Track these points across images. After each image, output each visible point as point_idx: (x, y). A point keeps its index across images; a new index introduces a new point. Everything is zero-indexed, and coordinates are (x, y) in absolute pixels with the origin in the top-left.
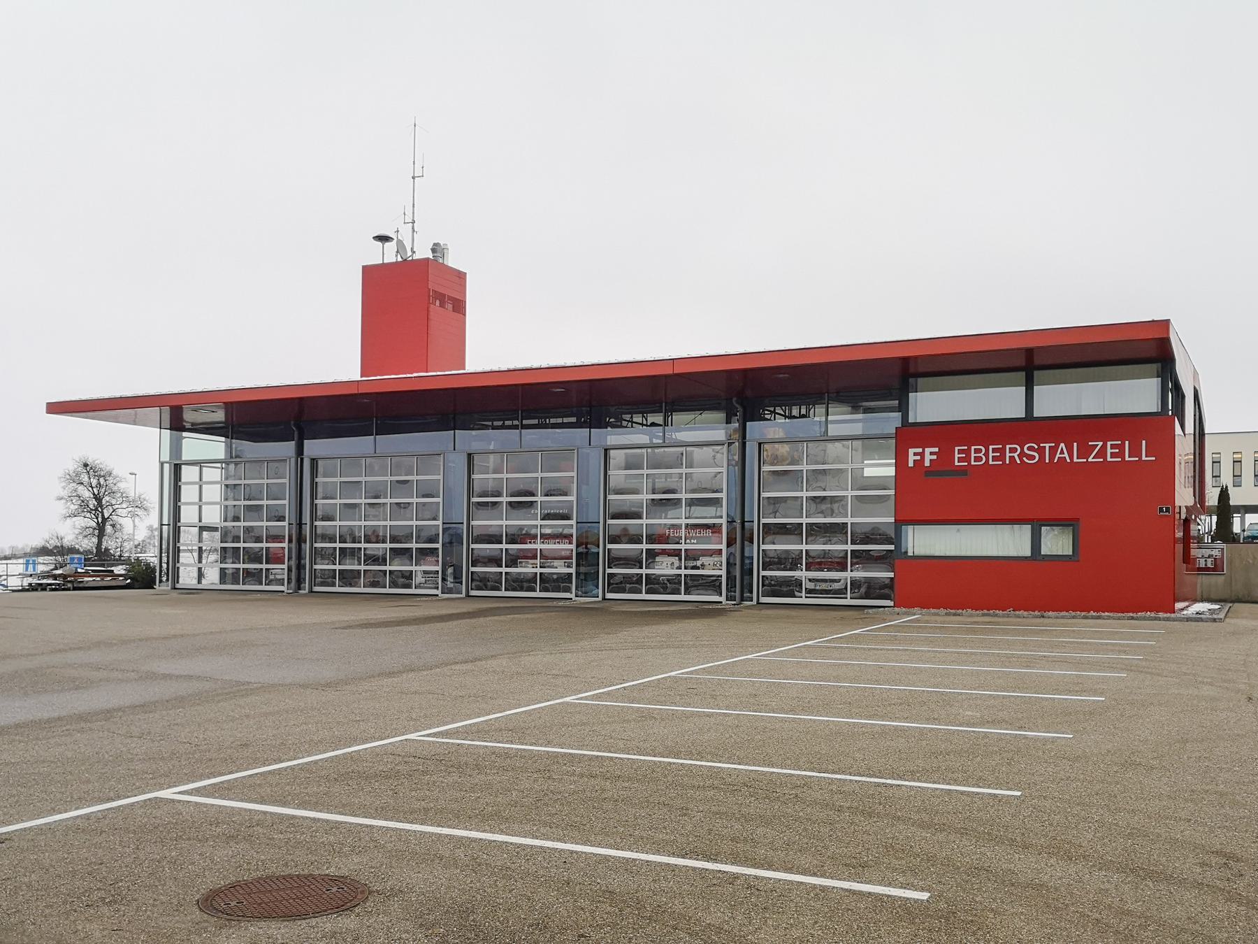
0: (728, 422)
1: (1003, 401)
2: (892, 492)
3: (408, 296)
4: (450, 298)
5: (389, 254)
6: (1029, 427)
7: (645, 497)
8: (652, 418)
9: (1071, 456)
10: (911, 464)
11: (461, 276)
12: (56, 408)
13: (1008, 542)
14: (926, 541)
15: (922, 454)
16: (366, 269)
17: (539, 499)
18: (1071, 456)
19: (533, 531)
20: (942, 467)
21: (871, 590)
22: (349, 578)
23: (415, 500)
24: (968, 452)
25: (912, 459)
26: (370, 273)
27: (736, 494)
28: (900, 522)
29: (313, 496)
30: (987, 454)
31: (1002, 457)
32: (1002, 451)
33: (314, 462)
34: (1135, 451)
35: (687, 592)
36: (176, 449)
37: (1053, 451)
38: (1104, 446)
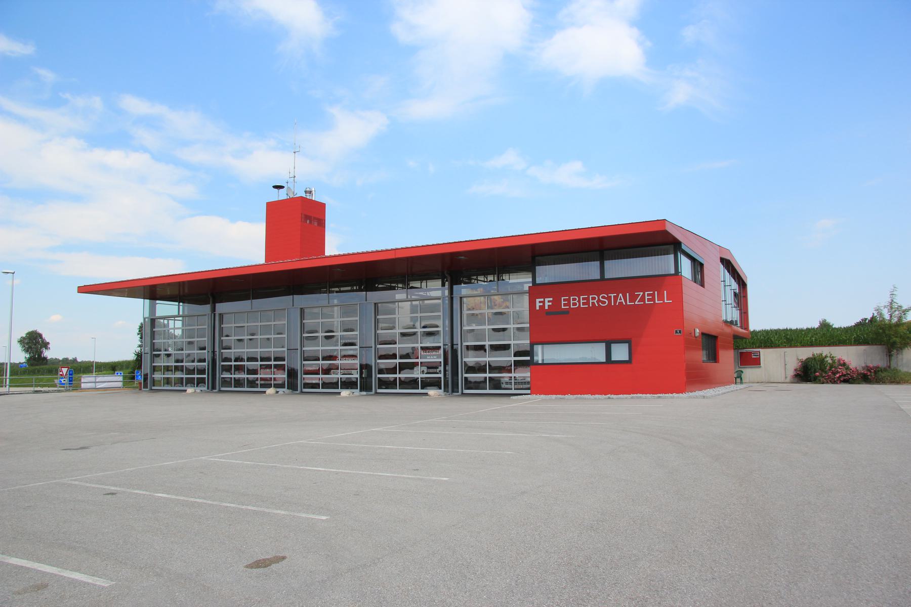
0: (443, 285)
1: (589, 270)
2: (528, 325)
3: (295, 218)
4: (315, 218)
5: (282, 195)
6: (603, 284)
7: (398, 331)
8: (490, 278)
9: (626, 302)
10: (538, 308)
11: (323, 206)
12: (83, 290)
13: (594, 353)
14: (546, 354)
15: (544, 302)
16: (268, 204)
18: (626, 302)
19: (335, 354)
20: (555, 310)
21: (180, 381)
22: (238, 383)
24: (569, 300)
25: (538, 305)
27: (448, 329)
28: (532, 344)
29: (221, 335)
30: (579, 301)
31: (588, 303)
33: (221, 315)
34: (661, 297)
35: (422, 388)
36: (153, 310)
37: (616, 298)
38: (644, 295)
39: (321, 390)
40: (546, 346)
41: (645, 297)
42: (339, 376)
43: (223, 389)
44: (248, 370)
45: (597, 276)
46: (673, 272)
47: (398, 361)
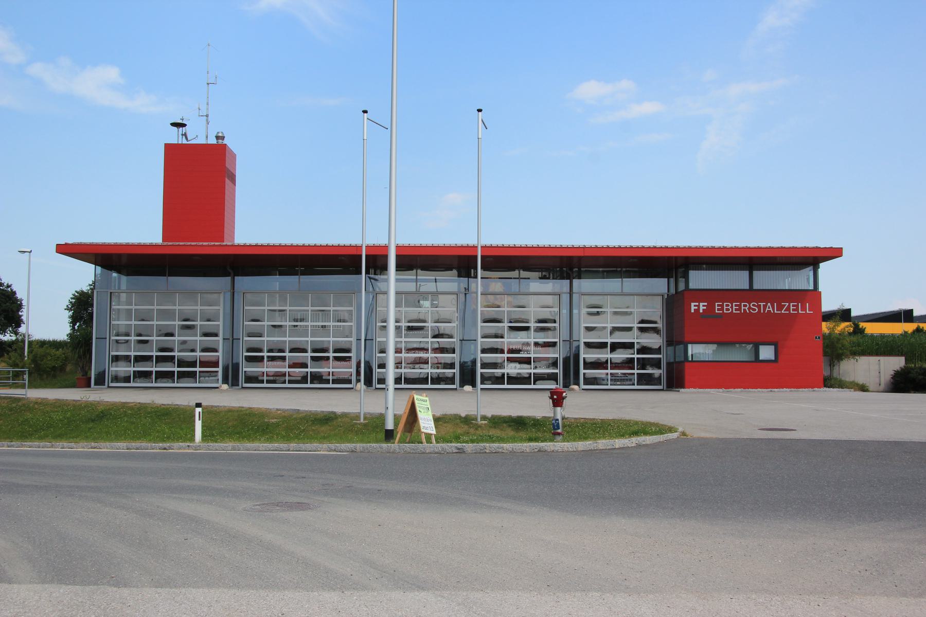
1: (736, 280)
6: (751, 294)
15: (698, 306)
17: (636, 325)
22: (169, 375)
23: (331, 324)
24: (722, 306)
26: (170, 149)
30: (732, 307)
31: (740, 309)
32: (740, 306)
34: (804, 308)
37: (765, 307)
38: (789, 306)
39: (429, 386)
40: (694, 345)
41: (790, 307)
42: (430, 371)
43: (111, 385)
44: (529, 363)
45: (414, 290)
46: (811, 287)
47: (506, 355)
